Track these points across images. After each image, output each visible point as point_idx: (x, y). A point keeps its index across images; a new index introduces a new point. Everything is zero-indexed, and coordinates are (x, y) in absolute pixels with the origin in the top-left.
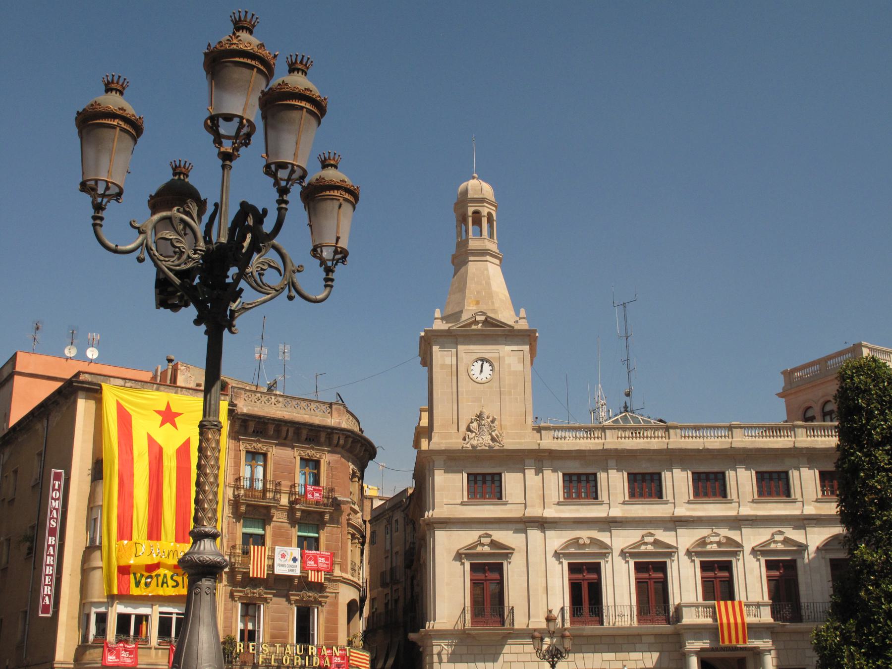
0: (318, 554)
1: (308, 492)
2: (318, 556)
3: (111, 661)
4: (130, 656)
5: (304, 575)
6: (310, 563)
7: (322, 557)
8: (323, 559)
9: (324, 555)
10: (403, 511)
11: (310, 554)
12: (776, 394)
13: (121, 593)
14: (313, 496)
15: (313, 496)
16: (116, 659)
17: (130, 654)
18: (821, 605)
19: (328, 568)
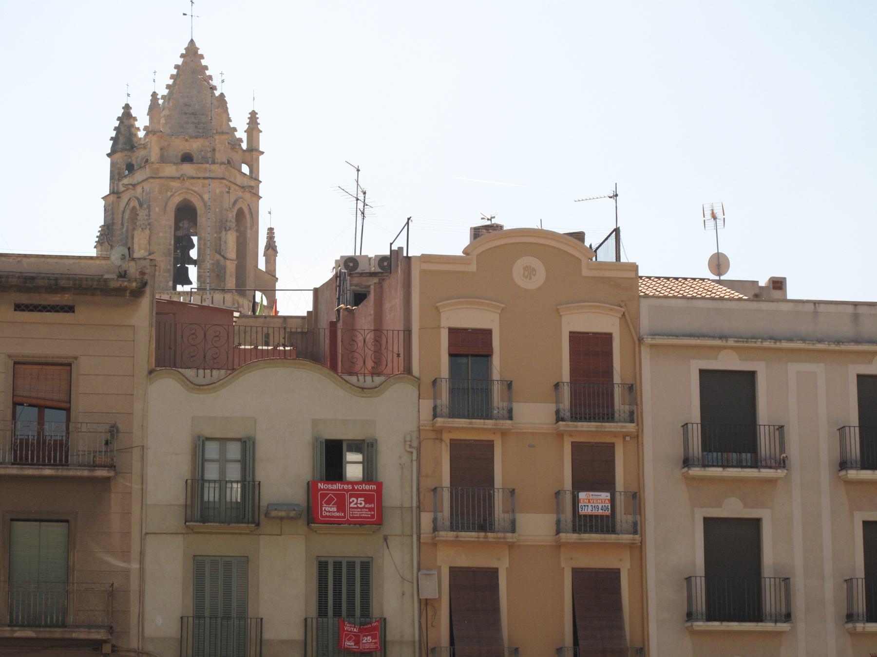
0: (348, 491)
1: (347, 635)
2: (347, 496)
3: (328, 514)
4: (366, 506)
5: (616, 415)
6: (327, 509)
7: (357, 496)
8: (361, 500)
9: (362, 490)
10: (249, 482)
11: (328, 490)
12: (192, 53)
13: (252, 147)
14: (357, 643)
15: (357, 643)
16: (338, 511)
17: (366, 502)
18: (772, 583)
19: (372, 516)
